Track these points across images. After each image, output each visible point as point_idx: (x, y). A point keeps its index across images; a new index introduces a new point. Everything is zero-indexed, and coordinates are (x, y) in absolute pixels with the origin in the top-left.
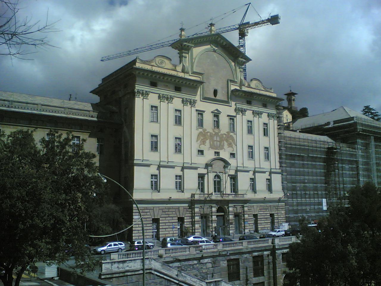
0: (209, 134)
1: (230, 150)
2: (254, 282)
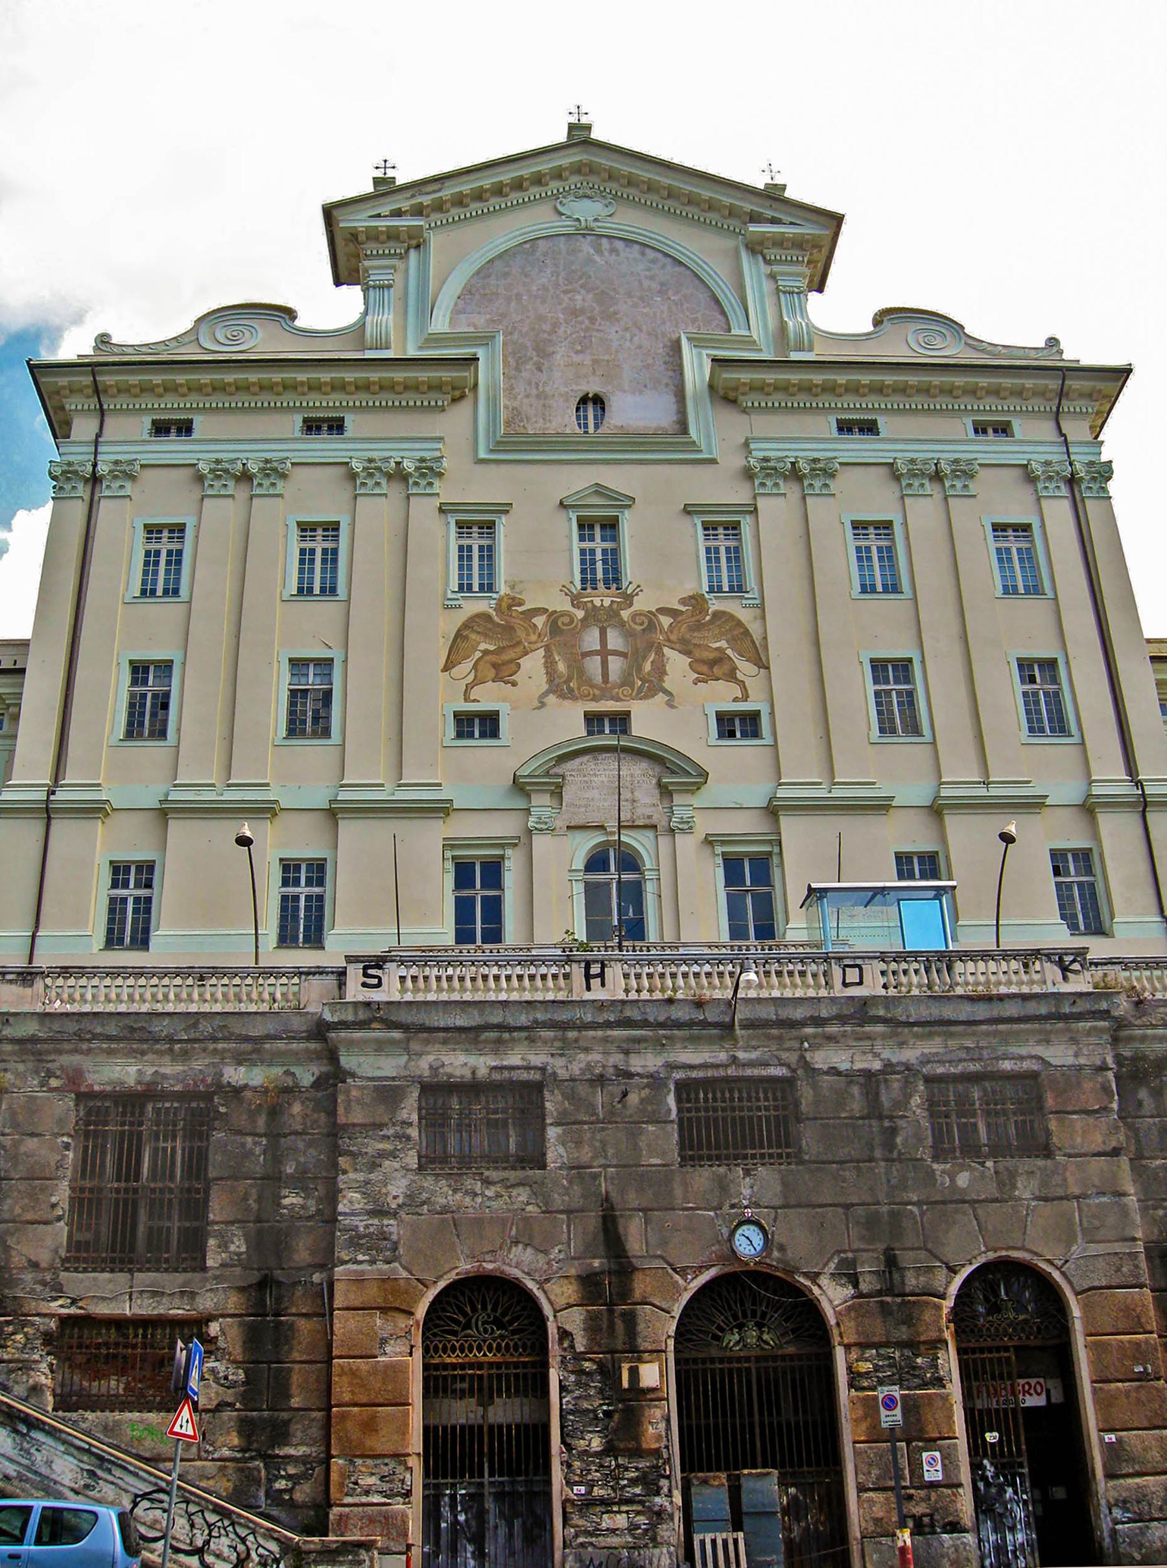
0: (540, 621)
1: (722, 697)
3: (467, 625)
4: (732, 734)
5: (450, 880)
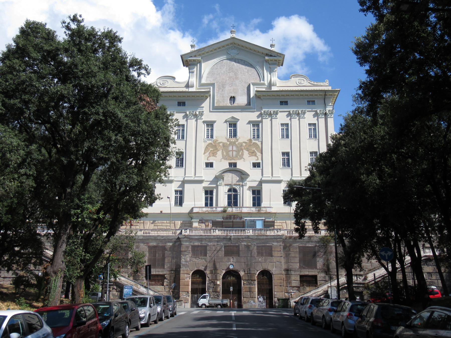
2: (226, 204)
3: (208, 145)
4: (255, 167)
5: (204, 194)
